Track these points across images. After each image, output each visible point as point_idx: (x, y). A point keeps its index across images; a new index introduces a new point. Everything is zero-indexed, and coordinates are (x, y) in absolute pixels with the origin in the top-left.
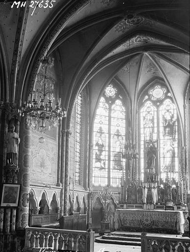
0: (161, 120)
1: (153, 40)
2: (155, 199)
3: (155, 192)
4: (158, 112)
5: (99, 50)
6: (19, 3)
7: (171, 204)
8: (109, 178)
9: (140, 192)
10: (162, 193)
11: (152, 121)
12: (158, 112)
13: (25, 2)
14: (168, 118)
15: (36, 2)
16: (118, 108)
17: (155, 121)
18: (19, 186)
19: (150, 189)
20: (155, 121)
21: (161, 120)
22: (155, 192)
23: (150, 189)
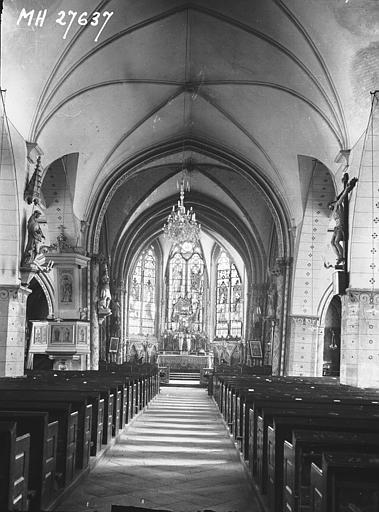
0: (189, 272)
1: (201, 158)
2: (189, 347)
3: (189, 341)
4: (187, 265)
5: (173, 161)
6: (32, 13)
7: (202, 351)
8: (141, 326)
9: (176, 341)
10: (194, 342)
11: (181, 273)
12: (187, 265)
13: (45, 11)
14: (196, 272)
15: (70, 12)
16: (224, 260)
17: (184, 274)
18: (87, 324)
19: (185, 339)
20: (184, 274)
21: (189, 272)
22: (189, 341)
23: (185, 339)
